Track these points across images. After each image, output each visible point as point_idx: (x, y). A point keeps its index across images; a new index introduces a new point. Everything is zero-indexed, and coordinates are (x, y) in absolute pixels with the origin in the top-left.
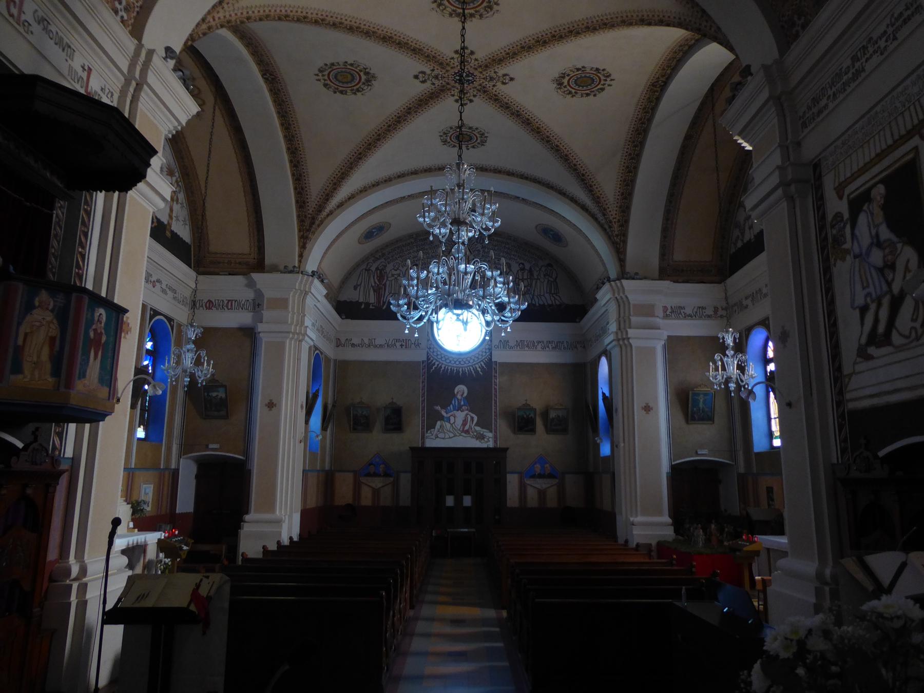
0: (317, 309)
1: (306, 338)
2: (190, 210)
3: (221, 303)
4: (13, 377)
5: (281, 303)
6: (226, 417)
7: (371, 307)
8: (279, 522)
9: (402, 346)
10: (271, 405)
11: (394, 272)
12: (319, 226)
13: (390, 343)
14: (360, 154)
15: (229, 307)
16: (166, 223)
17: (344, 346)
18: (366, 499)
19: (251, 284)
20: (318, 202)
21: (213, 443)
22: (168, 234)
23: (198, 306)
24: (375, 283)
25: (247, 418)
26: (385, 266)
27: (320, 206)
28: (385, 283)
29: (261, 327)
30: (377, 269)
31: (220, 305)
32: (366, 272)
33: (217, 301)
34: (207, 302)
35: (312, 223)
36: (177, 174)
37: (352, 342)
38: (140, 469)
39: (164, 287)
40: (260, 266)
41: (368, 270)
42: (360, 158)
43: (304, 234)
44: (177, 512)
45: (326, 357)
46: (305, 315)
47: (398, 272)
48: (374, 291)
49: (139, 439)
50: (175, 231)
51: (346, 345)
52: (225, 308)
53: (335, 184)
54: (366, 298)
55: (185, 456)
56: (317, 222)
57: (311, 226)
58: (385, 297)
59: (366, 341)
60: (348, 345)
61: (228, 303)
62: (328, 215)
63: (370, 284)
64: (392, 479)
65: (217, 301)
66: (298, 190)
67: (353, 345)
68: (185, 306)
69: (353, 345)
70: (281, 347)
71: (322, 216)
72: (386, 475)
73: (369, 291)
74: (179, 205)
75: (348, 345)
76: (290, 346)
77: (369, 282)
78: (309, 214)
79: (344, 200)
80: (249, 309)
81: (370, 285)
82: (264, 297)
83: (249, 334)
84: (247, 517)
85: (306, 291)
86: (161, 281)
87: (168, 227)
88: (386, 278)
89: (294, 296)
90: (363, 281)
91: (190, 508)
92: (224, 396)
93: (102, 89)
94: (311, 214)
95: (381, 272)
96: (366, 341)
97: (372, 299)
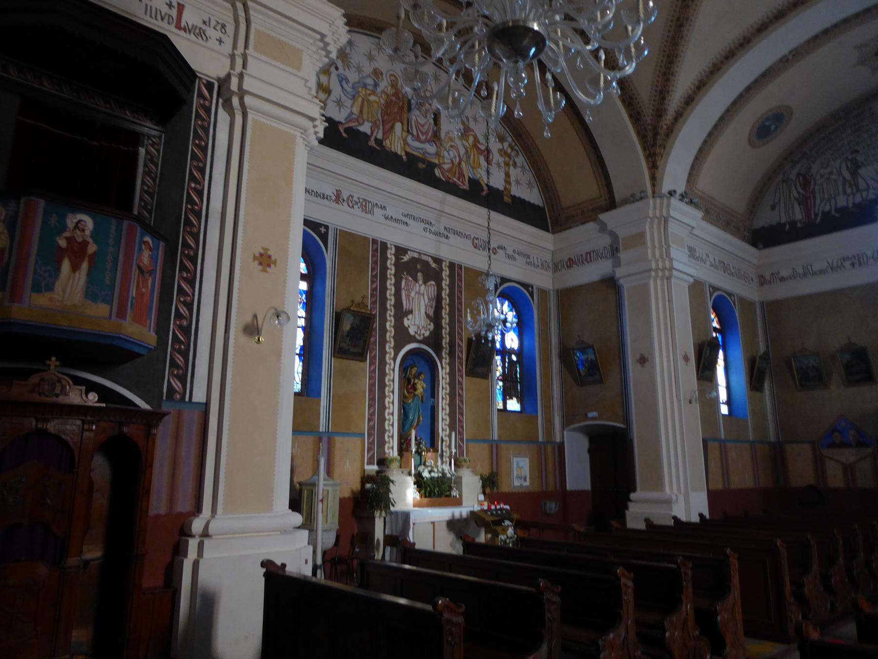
0: (700, 240)
1: (675, 273)
2: (534, 171)
3: (580, 258)
4: (34, 296)
5: (639, 239)
6: (601, 381)
7: (799, 225)
8: (668, 502)
9: (853, 265)
10: (643, 360)
11: (822, 171)
12: (668, 135)
13: (835, 264)
14: (678, 19)
15: (589, 260)
16: (501, 188)
17: (770, 282)
18: (835, 478)
19: (603, 228)
20: (653, 105)
21: (592, 411)
22: (507, 199)
23: (560, 268)
24: (799, 193)
25: (622, 378)
26: (809, 168)
27: (658, 110)
28: (814, 189)
29: (619, 273)
30: (799, 175)
31: (579, 261)
32: (784, 184)
33: (576, 258)
34: (567, 262)
35: (656, 134)
36: (510, 139)
37: (779, 276)
38: (508, 441)
39: (510, 252)
40: (612, 204)
41: (786, 181)
42: (682, 25)
43: (650, 152)
44: (568, 488)
45: (742, 300)
46: (669, 247)
47: (829, 169)
48: (799, 204)
49: (499, 410)
50: (517, 195)
51: (772, 282)
52: (585, 262)
53: (664, 74)
54: (789, 217)
55: (569, 428)
56: (662, 132)
57: (655, 139)
58: (817, 207)
59: (800, 270)
60: (775, 280)
61: (587, 256)
62: (676, 119)
63: (792, 196)
64: (869, 450)
65: (576, 258)
66: (627, 101)
67: (782, 279)
68: (546, 270)
69: (782, 279)
70: (645, 288)
71: (667, 122)
72: (860, 444)
73: (793, 207)
74: (519, 170)
75: (775, 280)
76: (655, 287)
77: (790, 195)
78: (648, 125)
79: (690, 92)
80: (608, 256)
81: (792, 198)
82: (618, 237)
83: (610, 283)
84: (633, 496)
85: (665, 218)
86: (504, 247)
87: (505, 193)
88: (812, 181)
89: (651, 228)
90: (782, 196)
91: (585, 484)
92: (593, 357)
93: (204, 22)
94: (651, 125)
95: (804, 177)
96: (800, 270)
97: (798, 214)
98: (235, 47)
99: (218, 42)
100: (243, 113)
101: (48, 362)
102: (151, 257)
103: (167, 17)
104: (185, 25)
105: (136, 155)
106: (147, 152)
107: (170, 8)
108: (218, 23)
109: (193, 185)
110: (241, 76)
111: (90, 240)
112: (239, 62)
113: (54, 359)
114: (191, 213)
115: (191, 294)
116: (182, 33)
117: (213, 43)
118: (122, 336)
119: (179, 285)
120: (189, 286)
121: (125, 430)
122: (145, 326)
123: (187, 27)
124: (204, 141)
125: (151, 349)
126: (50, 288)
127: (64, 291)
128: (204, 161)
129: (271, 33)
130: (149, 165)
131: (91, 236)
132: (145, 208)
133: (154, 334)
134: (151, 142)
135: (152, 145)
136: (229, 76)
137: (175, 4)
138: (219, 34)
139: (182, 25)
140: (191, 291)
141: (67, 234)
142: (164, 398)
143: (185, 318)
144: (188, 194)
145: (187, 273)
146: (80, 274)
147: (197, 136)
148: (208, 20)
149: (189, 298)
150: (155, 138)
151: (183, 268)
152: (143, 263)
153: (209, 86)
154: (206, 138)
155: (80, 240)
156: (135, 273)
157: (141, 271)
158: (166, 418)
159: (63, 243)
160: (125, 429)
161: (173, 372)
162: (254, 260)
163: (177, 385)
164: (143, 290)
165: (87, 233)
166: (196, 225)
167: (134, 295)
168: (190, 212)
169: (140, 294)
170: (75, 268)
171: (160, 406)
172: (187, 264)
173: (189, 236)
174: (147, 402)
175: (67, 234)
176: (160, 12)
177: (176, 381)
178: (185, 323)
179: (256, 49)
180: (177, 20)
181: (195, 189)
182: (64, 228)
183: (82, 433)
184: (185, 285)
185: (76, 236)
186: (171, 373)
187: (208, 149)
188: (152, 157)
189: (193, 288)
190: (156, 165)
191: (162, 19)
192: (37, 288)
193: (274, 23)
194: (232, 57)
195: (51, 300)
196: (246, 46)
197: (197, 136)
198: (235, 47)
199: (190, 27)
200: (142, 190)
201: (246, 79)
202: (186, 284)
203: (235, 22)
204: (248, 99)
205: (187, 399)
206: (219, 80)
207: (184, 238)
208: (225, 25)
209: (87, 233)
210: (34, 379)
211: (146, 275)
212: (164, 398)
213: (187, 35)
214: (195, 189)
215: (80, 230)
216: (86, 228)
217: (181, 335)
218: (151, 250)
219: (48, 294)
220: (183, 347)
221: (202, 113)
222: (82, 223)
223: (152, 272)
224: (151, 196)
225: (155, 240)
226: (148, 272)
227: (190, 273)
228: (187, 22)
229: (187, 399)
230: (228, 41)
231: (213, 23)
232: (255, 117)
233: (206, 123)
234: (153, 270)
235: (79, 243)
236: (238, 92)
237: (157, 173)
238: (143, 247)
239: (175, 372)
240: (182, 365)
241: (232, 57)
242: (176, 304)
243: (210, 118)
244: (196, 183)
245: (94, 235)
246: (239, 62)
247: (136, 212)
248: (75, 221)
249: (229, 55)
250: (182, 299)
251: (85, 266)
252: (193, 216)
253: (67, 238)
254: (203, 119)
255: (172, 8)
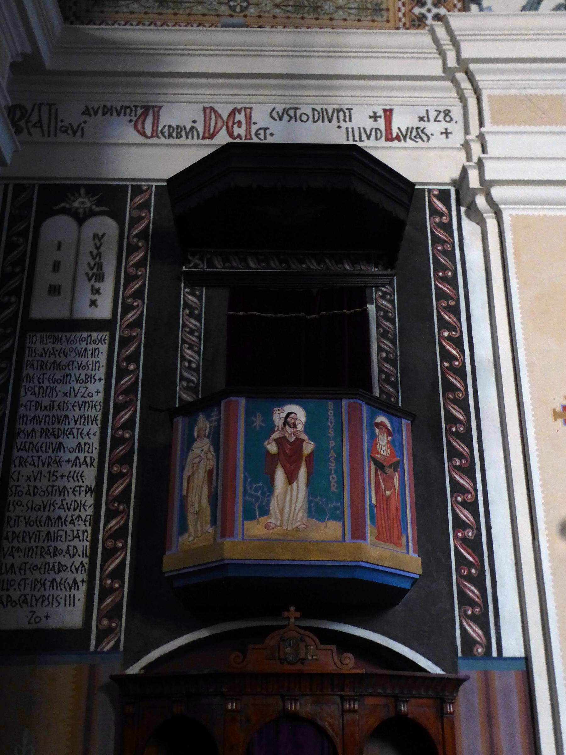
4: (247, 524)
98: (467, 131)
99: (444, 136)
100: (495, 213)
101: (286, 614)
102: (391, 444)
103: (373, 133)
104: (397, 133)
105: (365, 315)
106: (378, 308)
107: (375, 120)
108: (440, 112)
109: (446, 334)
110: (480, 164)
111: (304, 437)
112: (476, 148)
113: (292, 608)
114: (451, 374)
115: (472, 490)
116: (396, 143)
117: (438, 140)
118: (363, 564)
119: (452, 479)
120: (466, 478)
121: (403, 708)
122: (399, 545)
123: (399, 134)
124: (450, 270)
125: (416, 580)
126: (265, 511)
127: (282, 513)
128: (454, 297)
129: (513, 92)
130: (384, 324)
131: (306, 431)
132: (387, 381)
133: (416, 556)
134: (380, 293)
135: (383, 297)
136: (464, 171)
137: (380, 113)
138: (443, 125)
139: (394, 135)
140: (472, 484)
141: (276, 435)
142: (460, 654)
143: (470, 527)
144: (442, 347)
145: (460, 460)
146: (298, 484)
147: (438, 266)
148: (425, 115)
149: (470, 496)
150: (384, 287)
151: (454, 453)
152: (380, 454)
153: (444, 196)
154: (452, 265)
155: (293, 439)
156: (370, 470)
157: (379, 465)
158: (466, 684)
159: (272, 448)
160: (403, 708)
161: (465, 612)
162: (555, 420)
163: (475, 631)
164: (388, 493)
165: (300, 427)
166: (461, 387)
167: (374, 501)
168: (448, 371)
169: (384, 501)
170: (291, 478)
171: (454, 668)
172: (458, 446)
173: (453, 405)
174: (436, 663)
175: (276, 435)
176: (364, 129)
177: (472, 625)
178: (470, 534)
179: (495, 122)
180: (386, 130)
181: (449, 338)
182: (272, 428)
183: (342, 715)
184: (461, 477)
185: (286, 435)
186: (463, 614)
187: (457, 278)
188: (386, 312)
189: (473, 479)
190: (392, 321)
191: (368, 137)
192: (249, 515)
193: (510, 77)
194: (466, 146)
195: (267, 526)
196: (481, 124)
197: (438, 266)
198: (467, 131)
199: (404, 133)
200: (380, 359)
201: (488, 165)
202: (462, 475)
203: (461, 102)
204: (497, 192)
205: (495, 654)
206: (454, 183)
207: (447, 411)
208: (449, 111)
209: (300, 427)
210: (272, 641)
211: (390, 471)
212: (460, 654)
213: (403, 144)
214: (449, 338)
215: (290, 427)
216: (297, 422)
217: (468, 553)
218: (389, 434)
219: (263, 519)
220: (473, 571)
221: (442, 235)
222: (292, 416)
223: (397, 466)
224: (393, 363)
225: (395, 419)
226: (390, 467)
227: (465, 458)
228: (399, 128)
229: (495, 654)
230: (457, 129)
231: (432, 115)
232: (514, 213)
233: (449, 246)
234: (398, 462)
235: (292, 444)
236: (481, 187)
237: (396, 331)
238: (377, 431)
239: (470, 612)
240: (477, 599)
241: (466, 146)
242: (453, 509)
243: (452, 237)
244: (449, 331)
245: (309, 428)
246: (476, 148)
247: (377, 393)
248: (284, 415)
249: (462, 145)
250: (460, 499)
251: (302, 473)
252: (454, 376)
253: (275, 440)
254: (443, 242)
255: (378, 119)
